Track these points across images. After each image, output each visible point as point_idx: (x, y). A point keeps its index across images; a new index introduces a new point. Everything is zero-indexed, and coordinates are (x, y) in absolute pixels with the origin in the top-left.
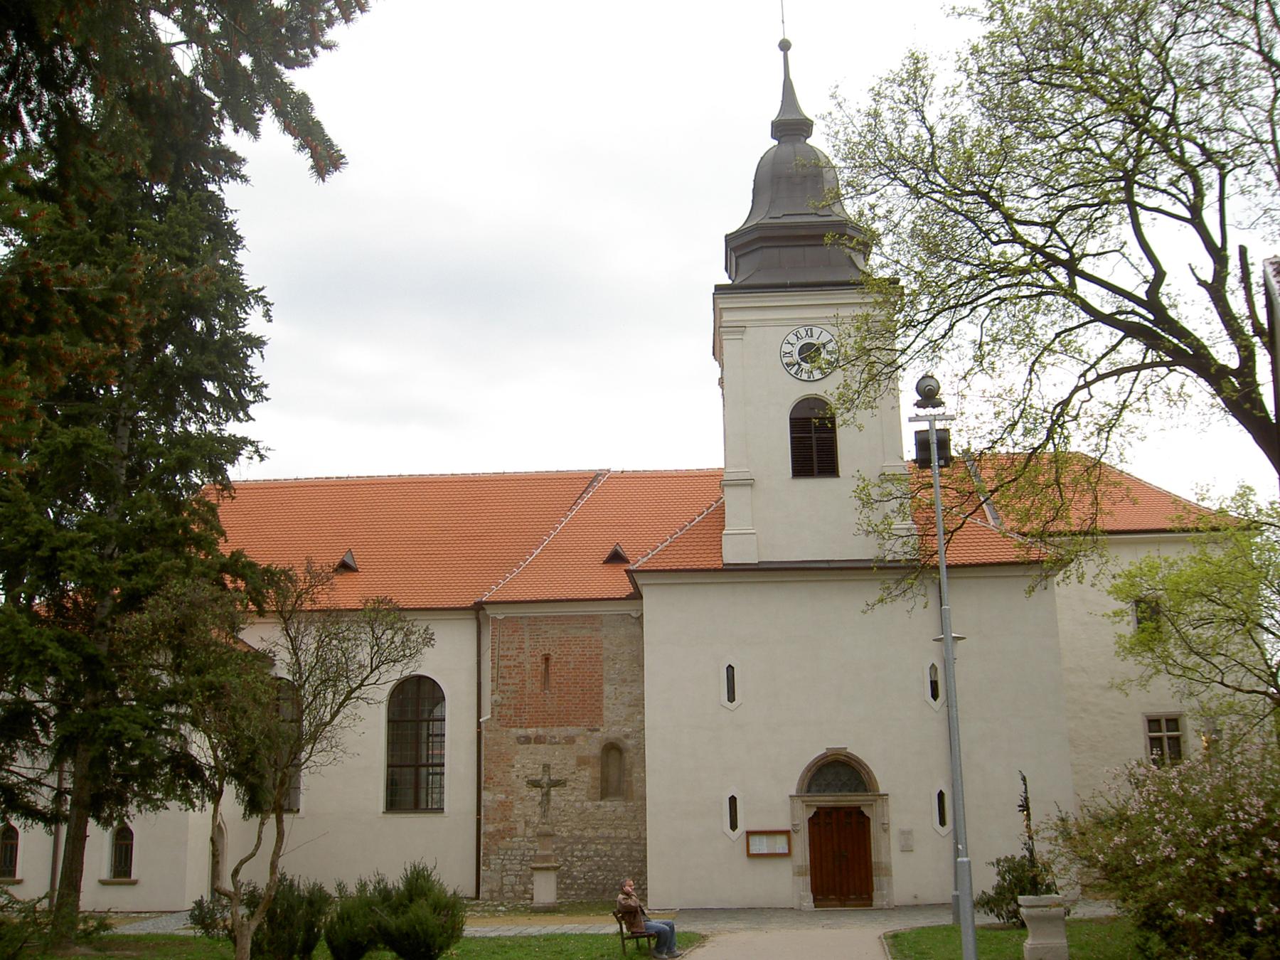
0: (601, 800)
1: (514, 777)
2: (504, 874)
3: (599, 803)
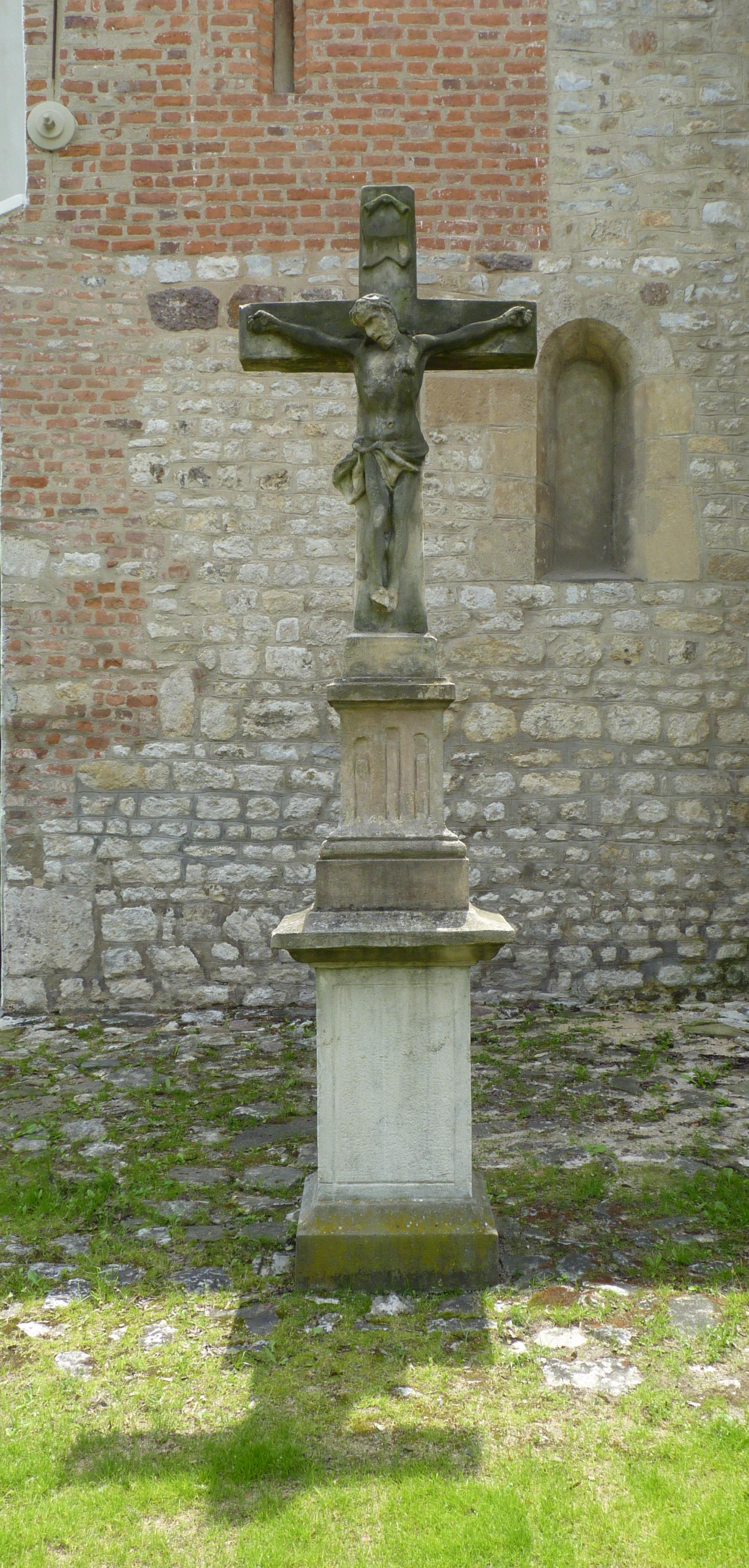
0: (538, 580)
1: (140, 475)
2: (106, 897)
3: (526, 591)
